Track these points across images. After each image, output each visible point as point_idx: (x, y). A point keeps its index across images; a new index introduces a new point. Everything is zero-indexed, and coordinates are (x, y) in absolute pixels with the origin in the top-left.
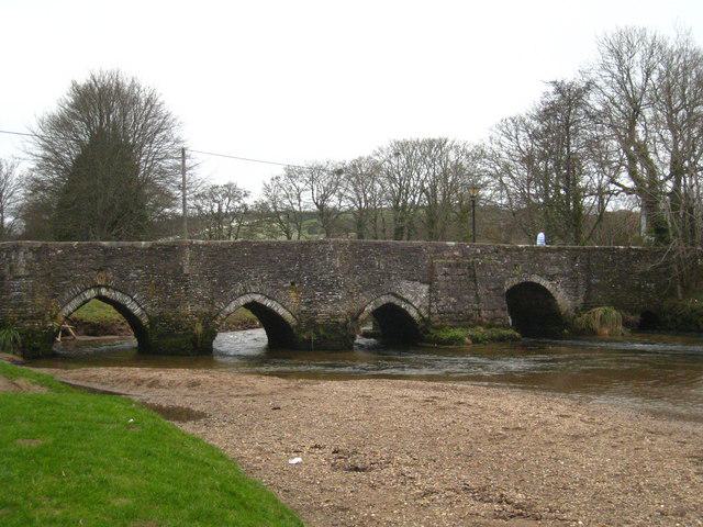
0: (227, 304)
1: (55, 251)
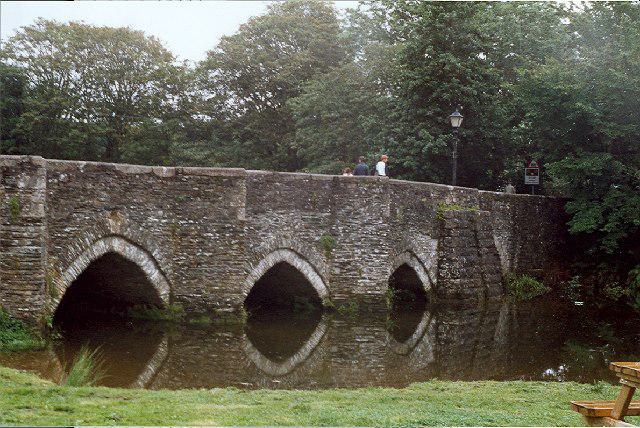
0: (256, 264)
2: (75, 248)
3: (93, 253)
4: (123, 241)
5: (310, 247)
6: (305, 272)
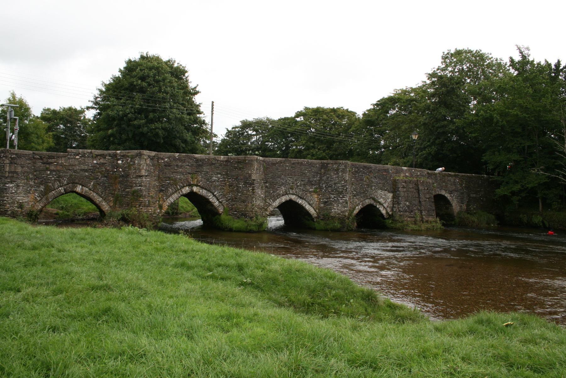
0: (274, 201)
1: (163, 159)
2: (172, 190)
3: (182, 192)
4: (198, 187)
5: (306, 194)
6: (304, 205)
